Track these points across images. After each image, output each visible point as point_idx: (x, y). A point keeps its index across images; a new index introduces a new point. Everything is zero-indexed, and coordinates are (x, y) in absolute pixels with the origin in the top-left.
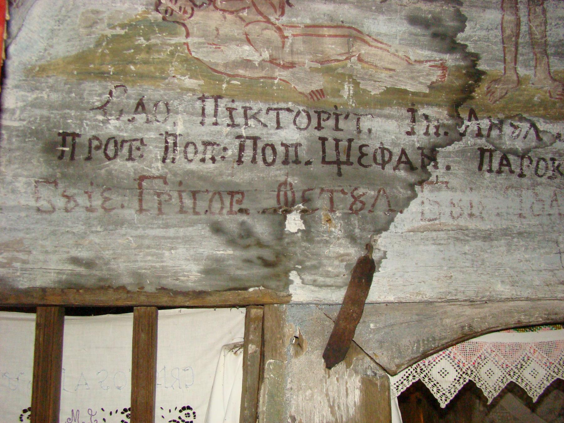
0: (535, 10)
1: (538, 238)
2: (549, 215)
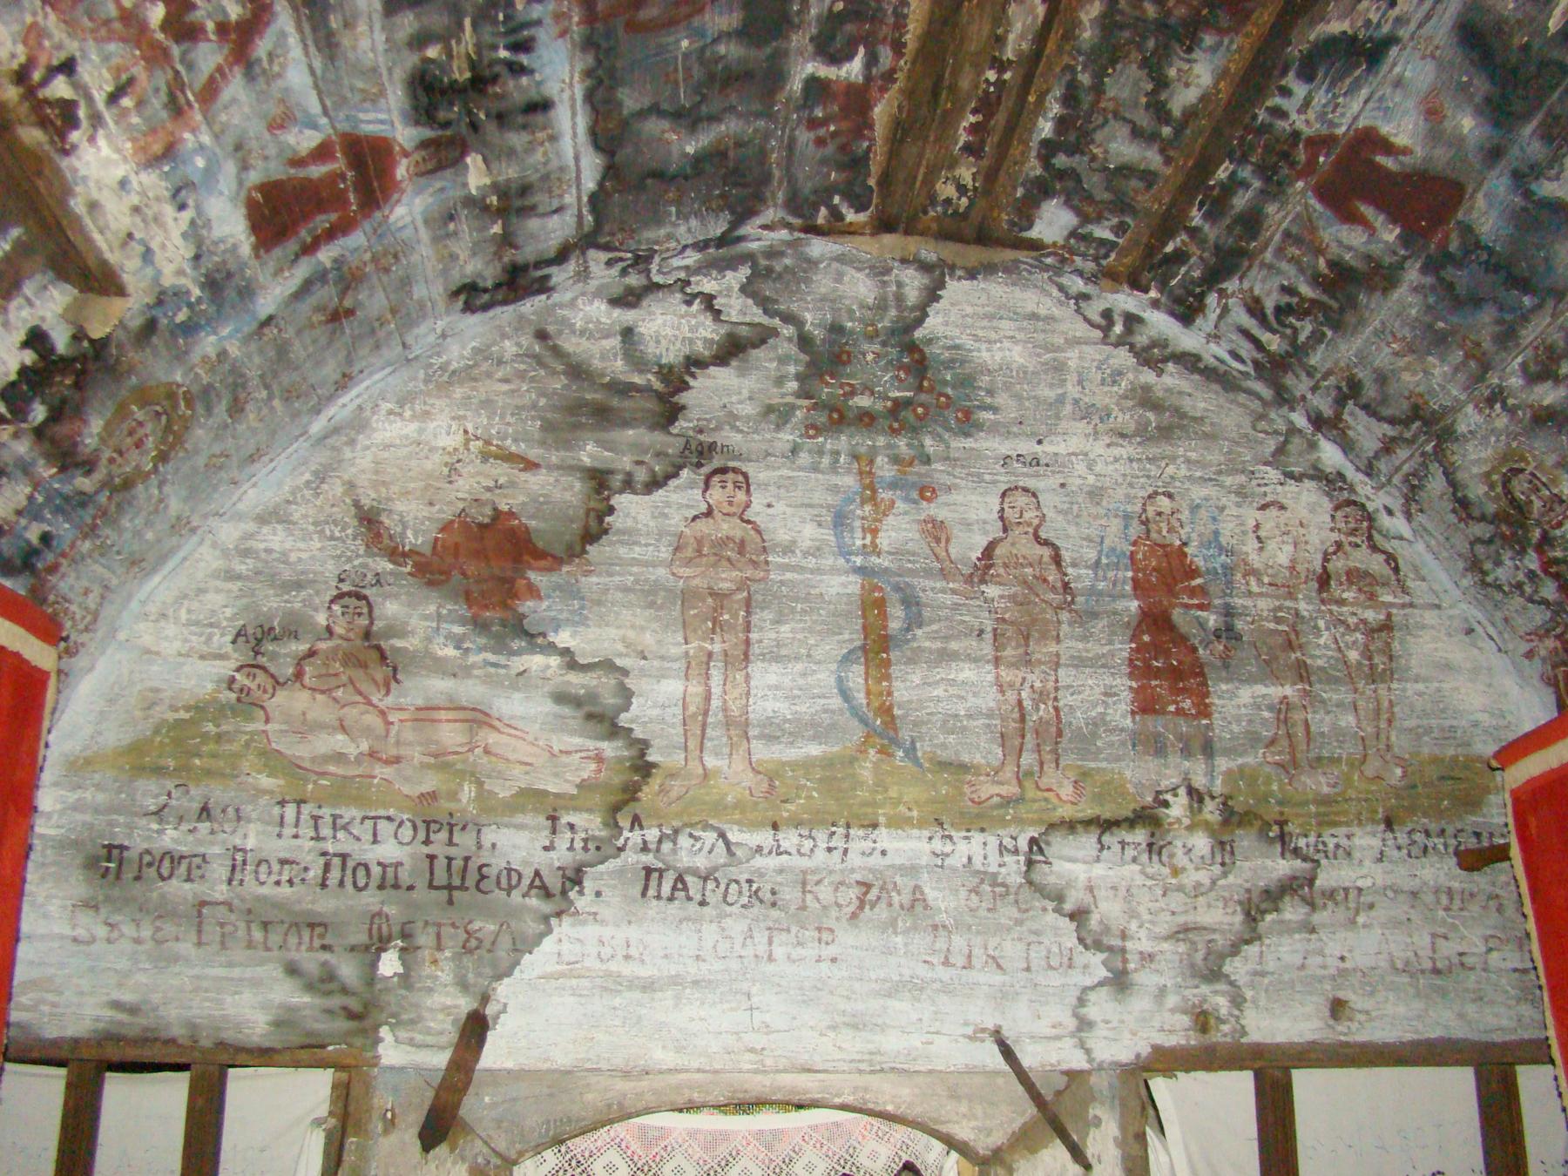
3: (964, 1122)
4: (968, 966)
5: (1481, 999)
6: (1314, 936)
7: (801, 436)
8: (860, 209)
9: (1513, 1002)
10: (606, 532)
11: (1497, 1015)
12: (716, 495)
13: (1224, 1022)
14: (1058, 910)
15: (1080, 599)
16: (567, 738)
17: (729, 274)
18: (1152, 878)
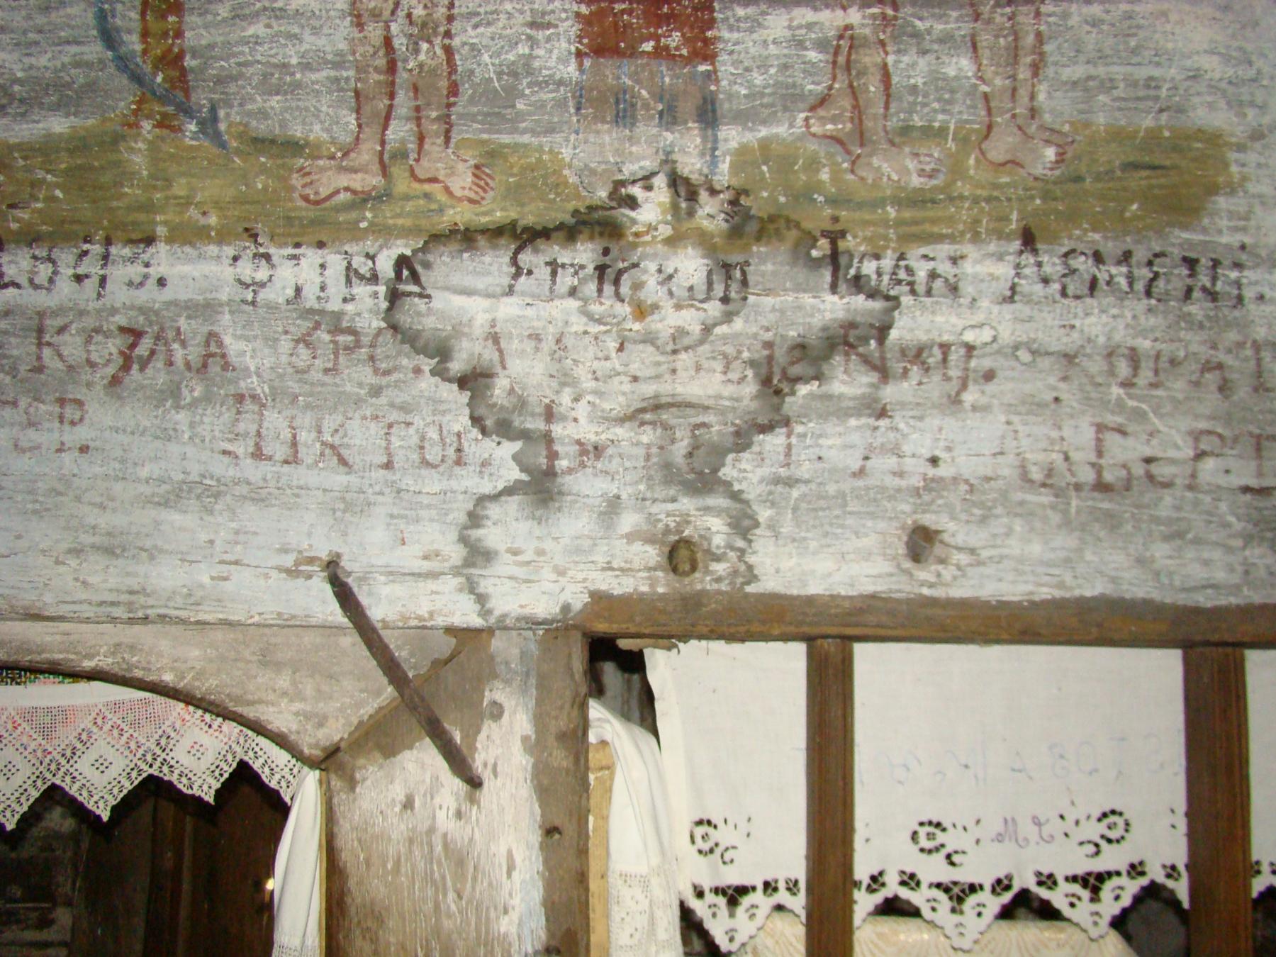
3: (284, 703)
4: (293, 459)
5: (1180, 535)
6: (883, 423)
9: (1238, 543)
11: (1206, 563)
13: (718, 559)
18: (600, 322)
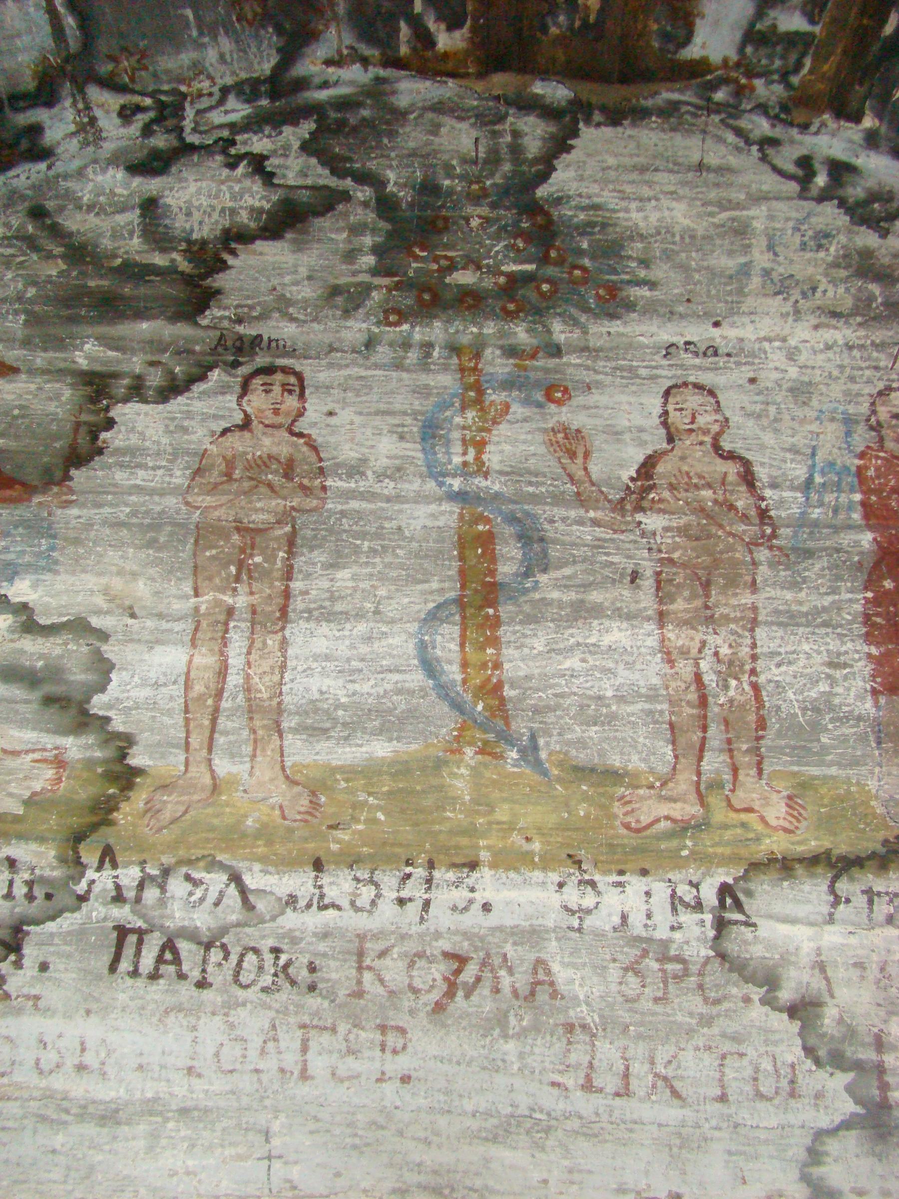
0: (265, 643)
1: (225, 1123)
2: (257, 1071)
4: (625, 1092)
7: (378, 323)
8: (453, 25)
10: (100, 452)
12: (257, 401)
14: (768, 1001)
15: (782, 531)
16: (15, 733)
17: (287, 130)
